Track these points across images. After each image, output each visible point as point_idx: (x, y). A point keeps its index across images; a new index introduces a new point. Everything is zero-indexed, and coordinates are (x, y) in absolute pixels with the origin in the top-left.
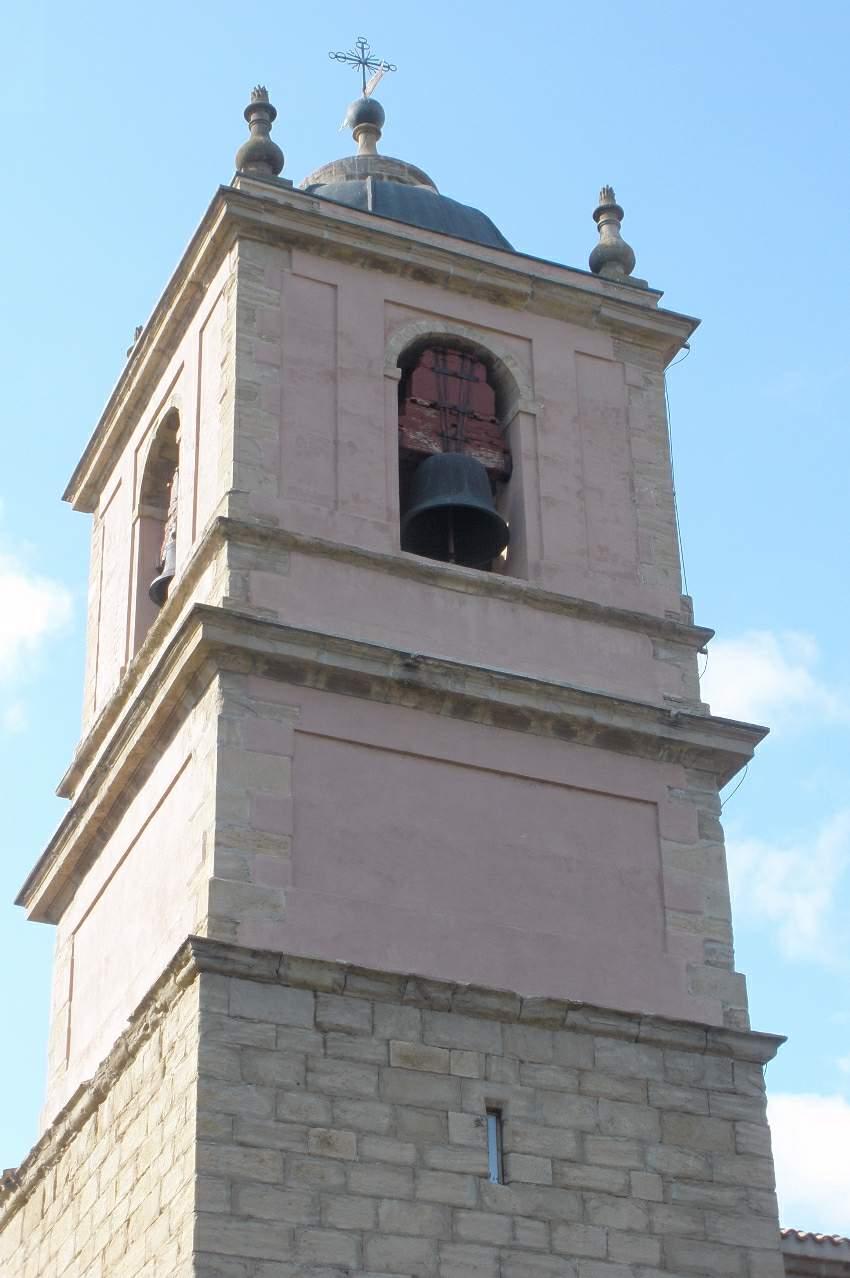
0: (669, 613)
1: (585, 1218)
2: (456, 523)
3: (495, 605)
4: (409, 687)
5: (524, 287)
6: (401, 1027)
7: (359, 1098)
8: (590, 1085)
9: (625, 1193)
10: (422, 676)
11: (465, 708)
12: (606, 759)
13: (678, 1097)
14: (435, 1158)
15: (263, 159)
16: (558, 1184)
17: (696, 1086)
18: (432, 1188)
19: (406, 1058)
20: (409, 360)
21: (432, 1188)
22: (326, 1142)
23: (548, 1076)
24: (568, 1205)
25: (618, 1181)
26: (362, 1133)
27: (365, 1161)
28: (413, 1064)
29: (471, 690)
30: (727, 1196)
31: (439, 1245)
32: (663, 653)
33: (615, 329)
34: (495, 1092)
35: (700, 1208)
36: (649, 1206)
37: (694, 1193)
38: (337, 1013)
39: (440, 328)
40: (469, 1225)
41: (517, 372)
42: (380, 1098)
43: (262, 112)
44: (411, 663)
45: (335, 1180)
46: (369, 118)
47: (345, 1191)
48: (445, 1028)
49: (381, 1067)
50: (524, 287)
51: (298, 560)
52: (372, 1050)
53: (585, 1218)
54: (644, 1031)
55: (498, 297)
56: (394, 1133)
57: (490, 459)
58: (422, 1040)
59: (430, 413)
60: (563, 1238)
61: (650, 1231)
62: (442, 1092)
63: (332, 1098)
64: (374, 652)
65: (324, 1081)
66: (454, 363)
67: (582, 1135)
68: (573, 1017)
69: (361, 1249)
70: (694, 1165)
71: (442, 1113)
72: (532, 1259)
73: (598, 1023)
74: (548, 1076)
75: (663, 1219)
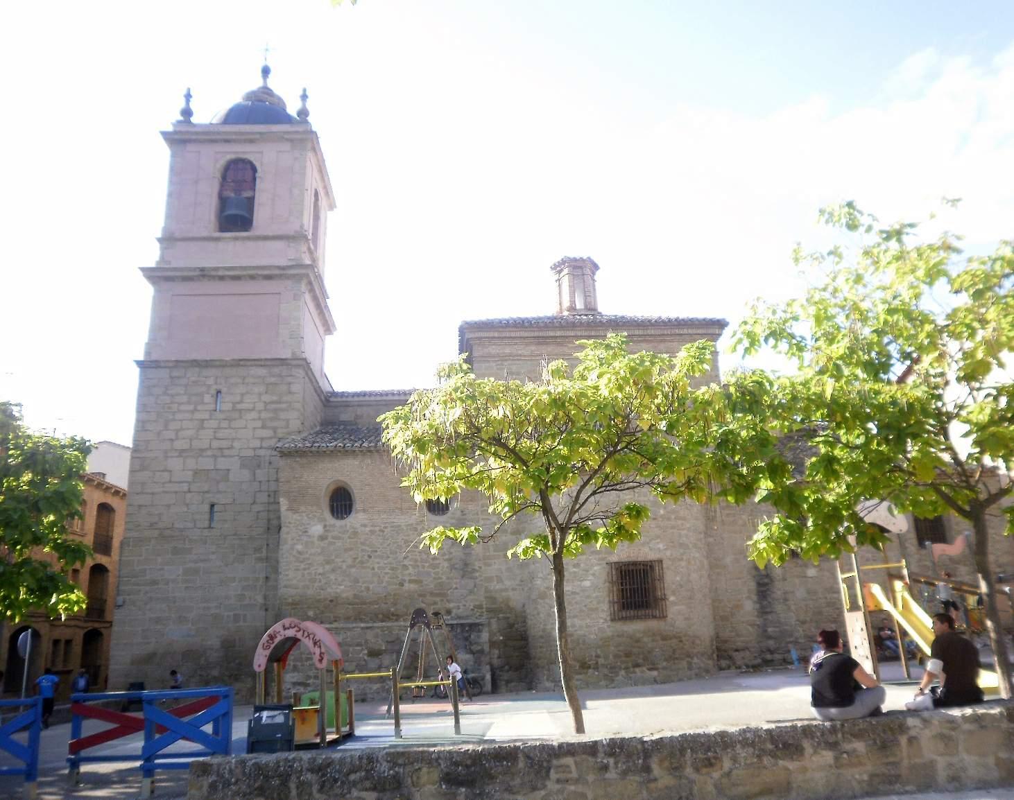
0: (296, 232)
1: (241, 418)
2: (235, 216)
3: (238, 243)
4: (204, 276)
5: (258, 136)
6: (192, 374)
7: (178, 394)
8: (246, 381)
9: (253, 409)
10: (206, 273)
11: (222, 278)
12: (266, 283)
13: (273, 380)
14: (199, 407)
15: (187, 113)
16: (234, 409)
17: (280, 376)
18: (198, 416)
19: (193, 382)
21: (198, 416)
22: (169, 408)
23: (233, 380)
24: (236, 415)
25: (251, 406)
26: (180, 404)
27: (179, 411)
29: (220, 273)
30: (284, 406)
32: (291, 245)
33: (291, 141)
34: (219, 387)
35: (276, 410)
36: (260, 412)
37: (274, 406)
38: (175, 373)
39: (233, 156)
40: (206, 424)
41: (257, 164)
43: (188, 96)
44: (202, 270)
45: (171, 417)
46: (266, 72)
47: (174, 420)
48: (206, 372)
50: (258, 136)
53: (241, 418)
54: (262, 363)
55: (251, 141)
56: (189, 403)
57: (247, 194)
58: (199, 376)
59: (232, 184)
60: (234, 424)
61: (259, 419)
62: (204, 389)
63: (172, 396)
64: (190, 269)
65: (170, 392)
66: (240, 166)
67: (242, 395)
68: (242, 363)
69: (177, 434)
70: (275, 398)
71: (201, 395)
72: (226, 431)
73: (249, 363)
74: (233, 380)
75: (264, 415)
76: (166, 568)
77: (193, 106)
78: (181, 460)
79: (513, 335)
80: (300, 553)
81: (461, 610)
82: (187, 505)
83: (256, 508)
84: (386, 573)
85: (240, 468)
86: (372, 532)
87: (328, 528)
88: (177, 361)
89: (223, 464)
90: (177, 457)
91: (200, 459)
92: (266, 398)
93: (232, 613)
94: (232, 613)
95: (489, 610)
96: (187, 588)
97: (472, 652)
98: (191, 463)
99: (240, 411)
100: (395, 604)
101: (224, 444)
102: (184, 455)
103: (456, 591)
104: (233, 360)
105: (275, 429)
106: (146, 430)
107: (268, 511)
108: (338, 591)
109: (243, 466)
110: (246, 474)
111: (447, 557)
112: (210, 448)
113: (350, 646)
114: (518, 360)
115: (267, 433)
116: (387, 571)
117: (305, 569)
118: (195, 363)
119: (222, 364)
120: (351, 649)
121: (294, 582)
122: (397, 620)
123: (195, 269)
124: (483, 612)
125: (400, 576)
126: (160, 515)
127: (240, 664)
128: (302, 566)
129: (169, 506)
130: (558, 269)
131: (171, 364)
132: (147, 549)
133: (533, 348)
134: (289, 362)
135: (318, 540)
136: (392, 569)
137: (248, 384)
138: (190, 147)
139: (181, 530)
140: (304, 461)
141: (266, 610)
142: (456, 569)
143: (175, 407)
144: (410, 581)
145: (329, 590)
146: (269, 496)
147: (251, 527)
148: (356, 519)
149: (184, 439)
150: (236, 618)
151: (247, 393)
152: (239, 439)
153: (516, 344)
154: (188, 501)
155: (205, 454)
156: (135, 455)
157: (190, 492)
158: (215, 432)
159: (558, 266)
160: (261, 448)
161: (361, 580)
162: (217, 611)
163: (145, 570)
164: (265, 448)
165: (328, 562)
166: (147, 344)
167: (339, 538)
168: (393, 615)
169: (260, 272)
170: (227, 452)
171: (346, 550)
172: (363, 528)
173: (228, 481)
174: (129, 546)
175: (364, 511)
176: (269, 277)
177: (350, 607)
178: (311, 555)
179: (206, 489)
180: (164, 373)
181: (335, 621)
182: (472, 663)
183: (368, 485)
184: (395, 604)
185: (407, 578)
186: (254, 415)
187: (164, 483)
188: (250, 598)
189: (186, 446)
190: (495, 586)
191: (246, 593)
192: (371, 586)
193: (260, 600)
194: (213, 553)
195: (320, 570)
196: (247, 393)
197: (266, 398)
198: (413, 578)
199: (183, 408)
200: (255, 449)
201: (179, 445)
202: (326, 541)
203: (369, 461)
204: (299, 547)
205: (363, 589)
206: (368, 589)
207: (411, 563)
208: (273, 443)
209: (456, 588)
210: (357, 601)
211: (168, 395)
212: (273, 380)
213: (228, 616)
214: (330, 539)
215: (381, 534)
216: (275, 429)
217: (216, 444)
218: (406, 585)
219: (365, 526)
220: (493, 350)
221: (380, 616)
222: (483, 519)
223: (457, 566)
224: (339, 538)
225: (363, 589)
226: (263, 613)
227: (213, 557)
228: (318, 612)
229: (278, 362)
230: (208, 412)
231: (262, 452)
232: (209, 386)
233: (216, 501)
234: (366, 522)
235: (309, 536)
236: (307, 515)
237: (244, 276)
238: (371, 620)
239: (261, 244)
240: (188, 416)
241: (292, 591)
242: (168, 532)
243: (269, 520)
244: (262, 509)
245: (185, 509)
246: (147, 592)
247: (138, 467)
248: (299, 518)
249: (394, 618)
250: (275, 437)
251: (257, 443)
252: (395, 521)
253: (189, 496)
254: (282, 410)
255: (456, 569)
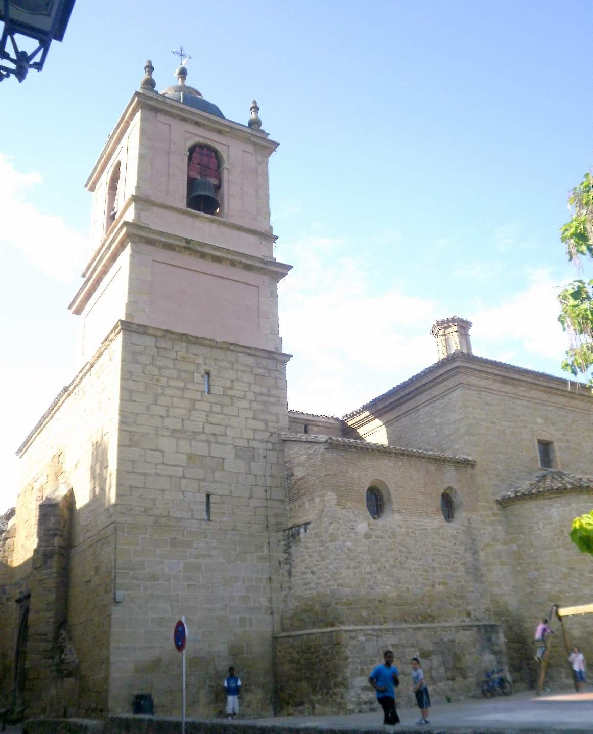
0: (266, 231)
2: (204, 200)
4: (186, 248)
6: (181, 349)
7: (168, 368)
9: (244, 398)
10: (191, 246)
11: (203, 256)
13: (261, 371)
14: (190, 386)
16: (225, 395)
20: (192, 150)
21: (188, 394)
22: (158, 381)
23: (223, 364)
24: (227, 401)
26: (168, 378)
27: (168, 386)
28: (184, 359)
31: (190, 410)
32: (264, 243)
34: (208, 368)
36: (251, 402)
37: (264, 398)
38: (162, 344)
40: (198, 405)
42: (174, 368)
43: (150, 68)
44: (188, 241)
46: (183, 73)
47: (163, 395)
48: (194, 349)
49: (175, 359)
50: (228, 130)
51: (155, 209)
52: (172, 355)
53: (232, 405)
59: (197, 166)
60: (226, 410)
61: (251, 409)
63: (160, 368)
65: (158, 363)
67: (232, 381)
68: (231, 347)
69: (167, 411)
70: (264, 391)
74: (223, 364)
76: (166, 561)
77: (154, 76)
78: (173, 441)
79: (490, 371)
80: (350, 550)
81: (477, 612)
82: (183, 492)
83: (254, 503)
84: (421, 575)
85: (236, 458)
86: (407, 534)
87: (371, 527)
88: (167, 331)
89: (216, 451)
90: (169, 437)
91: (193, 442)
92: (257, 389)
93: (237, 617)
94: (237, 617)
95: (496, 614)
96: (189, 586)
97: (495, 653)
98: (184, 445)
99: (232, 397)
100: (429, 605)
101: (218, 430)
102: (177, 435)
103: (472, 594)
104: (225, 342)
105: (266, 422)
106: (135, 401)
107: (267, 507)
108: (385, 591)
109: (237, 457)
110: (241, 466)
111: (462, 562)
112: (204, 432)
113: (405, 647)
114: (491, 393)
115: (260, 425)
116: (421, 572)
117: (355, 567)
118: (184, 337)
119: (213, 345)
120: (407, 650)
121: (347, 580)
122: (432, 622)
123: (181, 239)
124: (490, 615)
125: (431, 577)
126: (154, 500)
127: (249, 673)
128: (353, 564)
129: (163, 491)
130: (445, 325)
131: (160, 333)
132: (143, 538)
133: (499, 385)
134: (277, 356)
135: (364, 538)
136: (425, 571)
137: (237, 371)
138: (161, 117)
139: (178, 520)
140: (348, 456)
141: (272, 614)
142: (470, 573)
143: (164, 380)
144: (440, 583)
145: (378, 590)
146: (266, 491)
147: (249, 523)
148: (391, 520)
149: (175, 417)
150: (242, 621)
151: (237, 379)
152: (233, 427)
153: (488, 379)
154: (183, 488)
155: (198, 437)
156: (124, 427)
157: (184, 477)
158: (207, 416)
159: (445, 323)
160: (254, 439)
161: (402, 581)
162: (223, 614)
163: (143, 562)
164: (258, 440)
165: (375, 561)
166: (127, 305)
167: (381, 537)
168: (429, 616)
169: (244, 260)
170: (220, 439)
171: (388, 550)
172: (399, 529)
173: (223, 470)
174: (123, 531)
175: (400, 512)
176: (248, 268)
177: (397, 608)
178: (359, 553)
179: (202, 476)
180: (149, 341)
181: (385, 622)
182: (495, 663)
183: (402, 487)
184: (429, 605)
185: (437, 580)
186: (244, 404)
187: (156, 465)
188: (255, 600)
189: (179, 426)
190: (496, 590)
191: (250, 595)
192: (410, 587)
193: (264, 603)
194: (214, 548)
195: (368, 569)
196: (237, 379)
197: (257, 389)
198: (441, 580)
199: (172, 383)
200: (248, 440)
201: (171, 423)
202: (371, 540)
203: (401, 464)
204: (349, 544)
205: (404, 589)
206: (408, 589)
207: (438, 566)
208: (266, 435)
209: (472, 592)
210: (401, 601)
211: (156, 366)
212: (261, 371)
213: (235, 620)
214: (374, 538)
215: (413, 535)
216: (266, 422)
217: (209, 429)
218: (437, 587)
219: (401, 527)
220: (473, 380)
221: (420, 618)
222: (483, 528)
223: (470, 570)
224: (381, 537)
225: (404, 589)
226: (269, 617)
227: (214, 553)
228: (370, 612)
229: (266, 355)
230: (199, 393)
231: (256, 445)
232: (198, 365)
233: (212, 491)
234: (401, 523)
235: (356, 533)
236: (354, 512)
237: (227, 259)
238: (413, 621)
239: (236, 233)
240: (179, 393)
241: (347, 591)
242: (163, 521)
243: (267, 516)
244: (258, 505)
245: (181, 497)
246: (146, 589)
247: (127, 443)
248: (347, 514)
249: (430, 619)
250: (266, 430)
251: (250, 435)
252: (423, 524)
253: (184, 481)
254: (271, 404)
255: (470, 573)
